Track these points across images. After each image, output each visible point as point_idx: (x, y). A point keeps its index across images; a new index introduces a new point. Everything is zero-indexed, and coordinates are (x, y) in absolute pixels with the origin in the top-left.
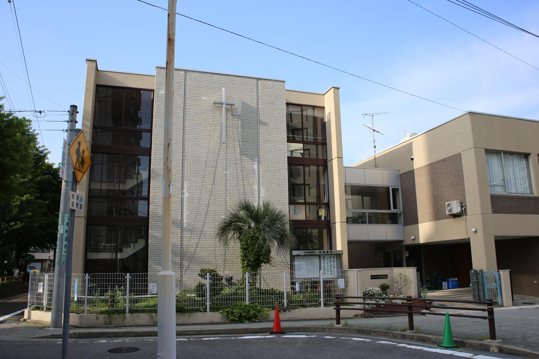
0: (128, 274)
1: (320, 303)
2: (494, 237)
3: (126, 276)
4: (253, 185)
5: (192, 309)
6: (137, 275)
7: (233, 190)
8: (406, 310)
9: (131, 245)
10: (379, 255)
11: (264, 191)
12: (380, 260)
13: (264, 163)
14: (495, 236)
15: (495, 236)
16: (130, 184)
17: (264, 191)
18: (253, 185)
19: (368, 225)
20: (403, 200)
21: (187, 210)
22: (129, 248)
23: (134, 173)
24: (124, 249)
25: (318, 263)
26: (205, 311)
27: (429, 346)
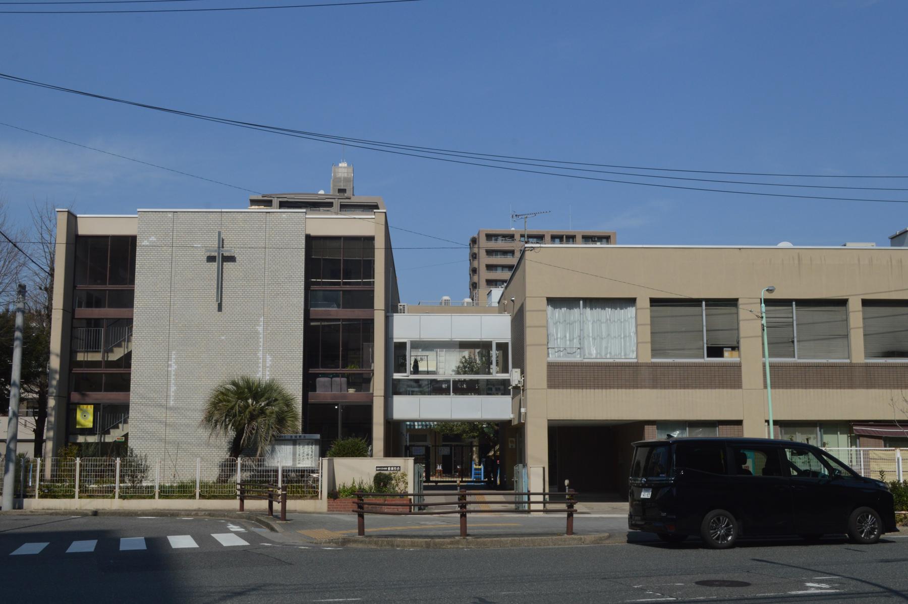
0: (118, 459)
1: (195, 495)
2: (547, 421)
3: (116, 460)
4: (257, 352)
5: (98, 495)
6: (92, 459)
7: (218, 359)
8: (368, 508)
9: (120, 425)
10: (514, 439)
11: (271, 359)
12: (514, 447)
13: (272, 323)
14: (548, 420)
15: (548, 420)
16: (116, 355)
17: (271, 359)
18: (257, 352)
19: (451, 397)
20: (797, 329)
21: (174, 386)
22: (118, 430)
23: (124, 340)
24: (111, 431)
25: (416, 447)
26: (114, 497)
27: (66, 515)
